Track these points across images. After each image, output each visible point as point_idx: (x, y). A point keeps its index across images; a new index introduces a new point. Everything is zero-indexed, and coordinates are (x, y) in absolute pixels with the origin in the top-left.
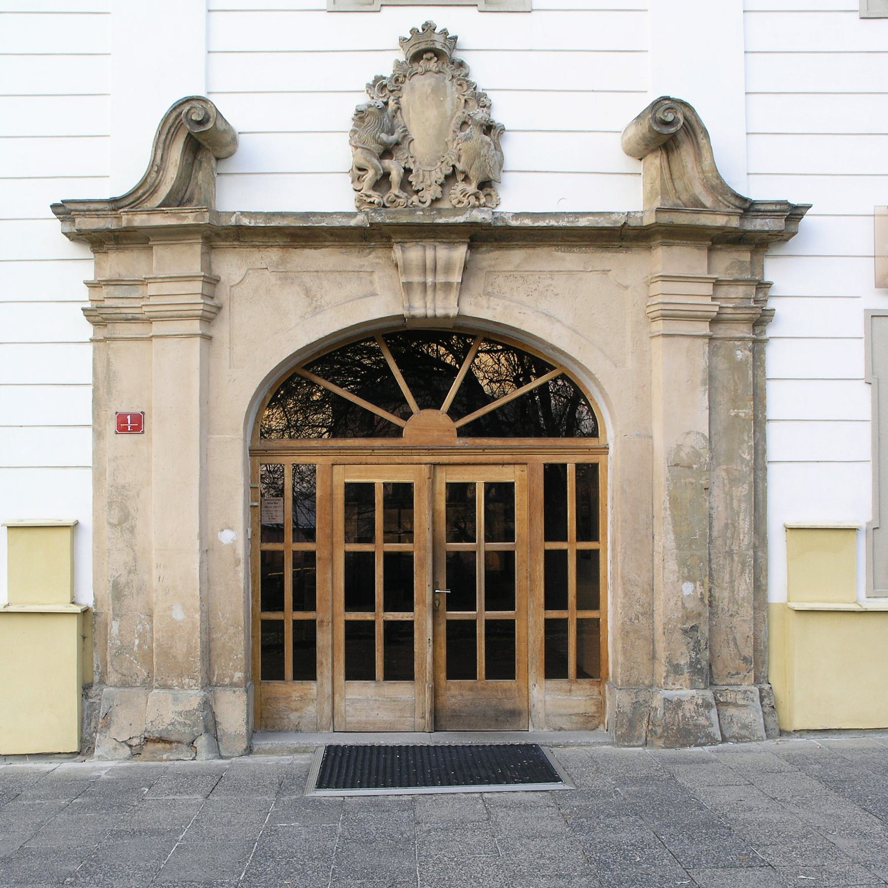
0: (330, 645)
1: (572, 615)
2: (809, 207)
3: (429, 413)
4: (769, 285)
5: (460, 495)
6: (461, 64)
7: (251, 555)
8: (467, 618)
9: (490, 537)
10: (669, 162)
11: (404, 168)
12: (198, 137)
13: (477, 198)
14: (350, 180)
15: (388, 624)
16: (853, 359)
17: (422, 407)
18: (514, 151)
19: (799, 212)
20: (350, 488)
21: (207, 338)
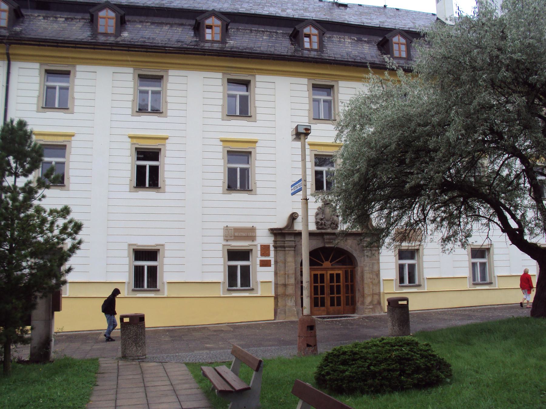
0: (328, 302)
1: (350, 295)
5: (332, 276)
21: (294, 250)
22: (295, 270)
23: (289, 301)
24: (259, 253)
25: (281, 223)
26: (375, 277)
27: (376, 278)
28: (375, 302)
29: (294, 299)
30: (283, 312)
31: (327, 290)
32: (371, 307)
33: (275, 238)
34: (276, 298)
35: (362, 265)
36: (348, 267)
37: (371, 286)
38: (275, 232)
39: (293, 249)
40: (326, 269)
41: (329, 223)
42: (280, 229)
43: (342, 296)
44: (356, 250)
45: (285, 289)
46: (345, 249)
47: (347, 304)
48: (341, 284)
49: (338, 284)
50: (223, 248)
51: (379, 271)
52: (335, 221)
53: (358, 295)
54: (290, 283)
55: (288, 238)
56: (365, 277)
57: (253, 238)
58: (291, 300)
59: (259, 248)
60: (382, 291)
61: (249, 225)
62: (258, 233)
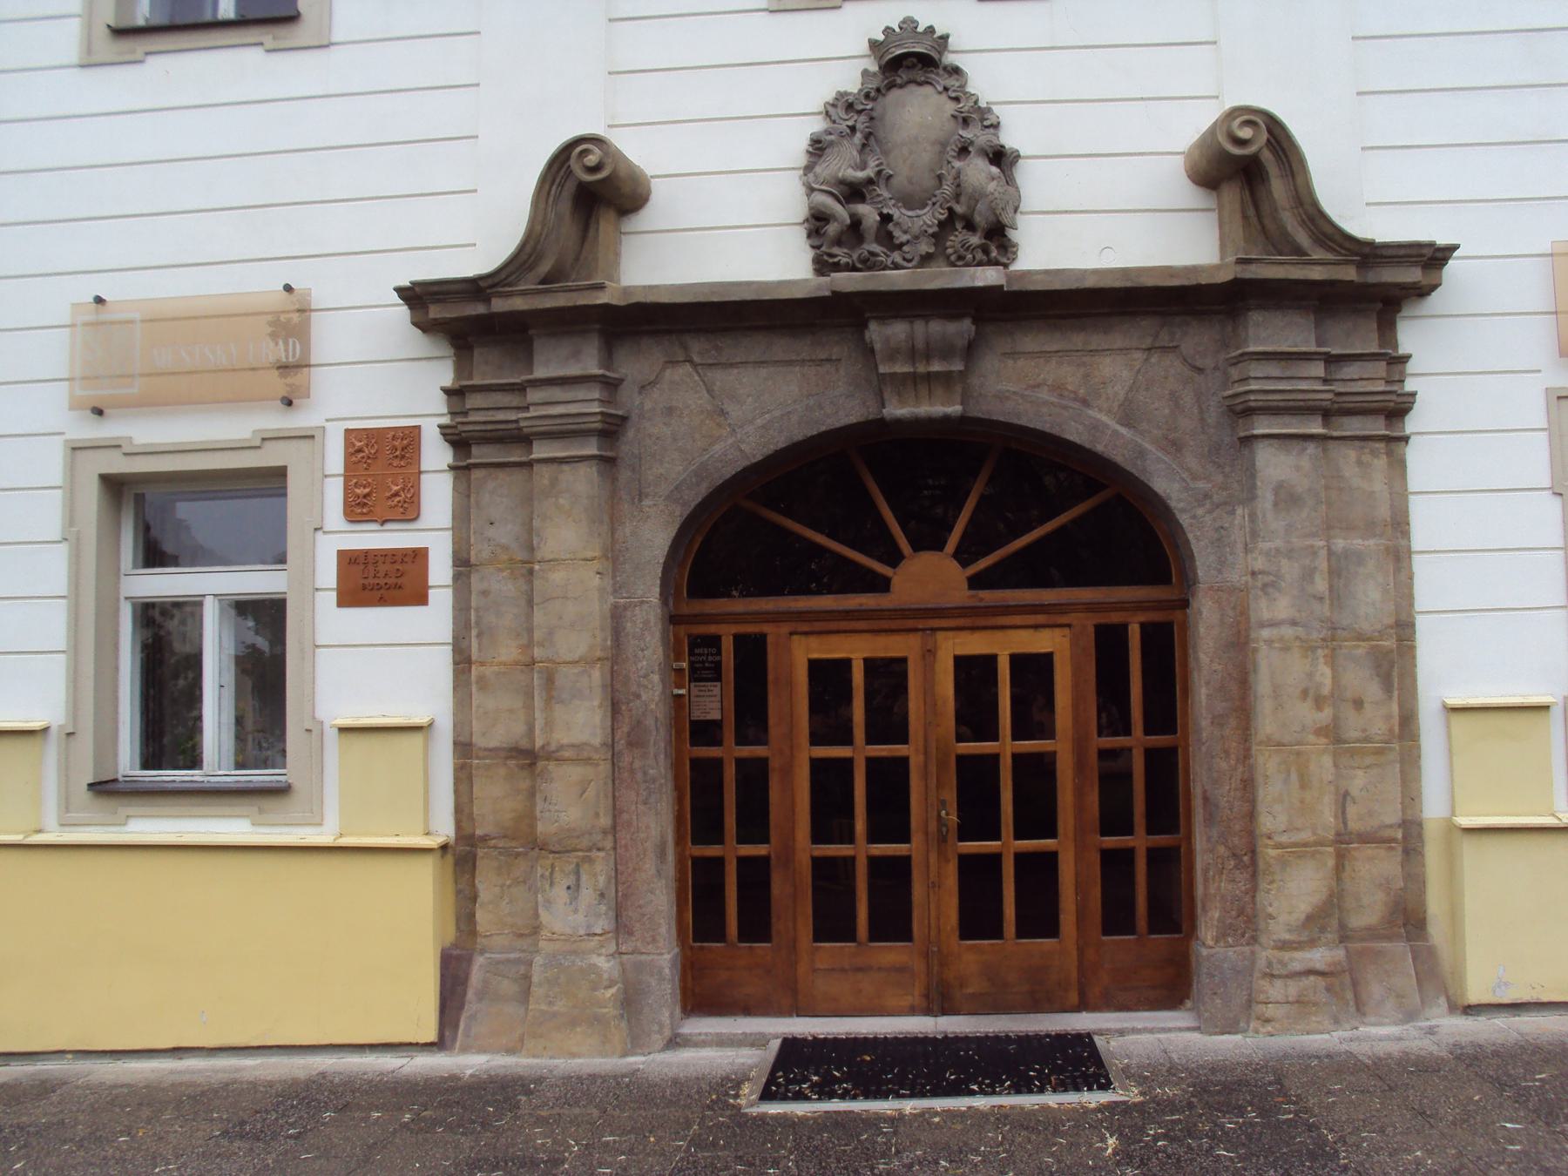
0: (936, 898)
2: (1455, 248)
3: (928, 558)
4: (1405, 359)
5: (974, 675)
6: (956, 71)
7: (676, 766)
8: (1031, 849)
9: (718, 764)
10: (1252, 194)
11: (881, 214)
12: (590, 191)
13: (986, 251)
14: (804, 234)
15: (874, 862)
16: (1532, 460)
17: (917, 547)
18: (1034, 182)
19: (1439, 255)
20: (815, 667)
21: (608, 463)
22: (617, 633)
23: (560, 893)
24: (334, 493)
25: (480, 231)
26: (1361, 680)
27: (1373, 690)
28: (1368, 910)
29: (599, 873)
30: (507, 987)
31: (931, 800)
32: (1319, 957)
33: (461, 369)
34: (462, 856)
35: (1235, 577)
36: (1127, 602)
37: (1323, 766)
38: (435, 312)
39: (591, 448)
40: (926, 618)
41: (928, 218)
42: (475, 288)
43: (1074, 853)
44: (1174, 446)
45: (532, 793)
46: (1074, 433)
47: (1117, 918)
48: (1061, 746)
49: (1028, 745)
50: (71, 470)
51: (1404, 629)
52: (977, 197)
53: (1206, 849)
54: (562, 737)
55: (551, 361)
56: (1263, 684)
57: (291, 377)
58: (574, 889)
59: (335, 459)
60: (1433, 807)
61: (263, 283)
62: (331, 340)
